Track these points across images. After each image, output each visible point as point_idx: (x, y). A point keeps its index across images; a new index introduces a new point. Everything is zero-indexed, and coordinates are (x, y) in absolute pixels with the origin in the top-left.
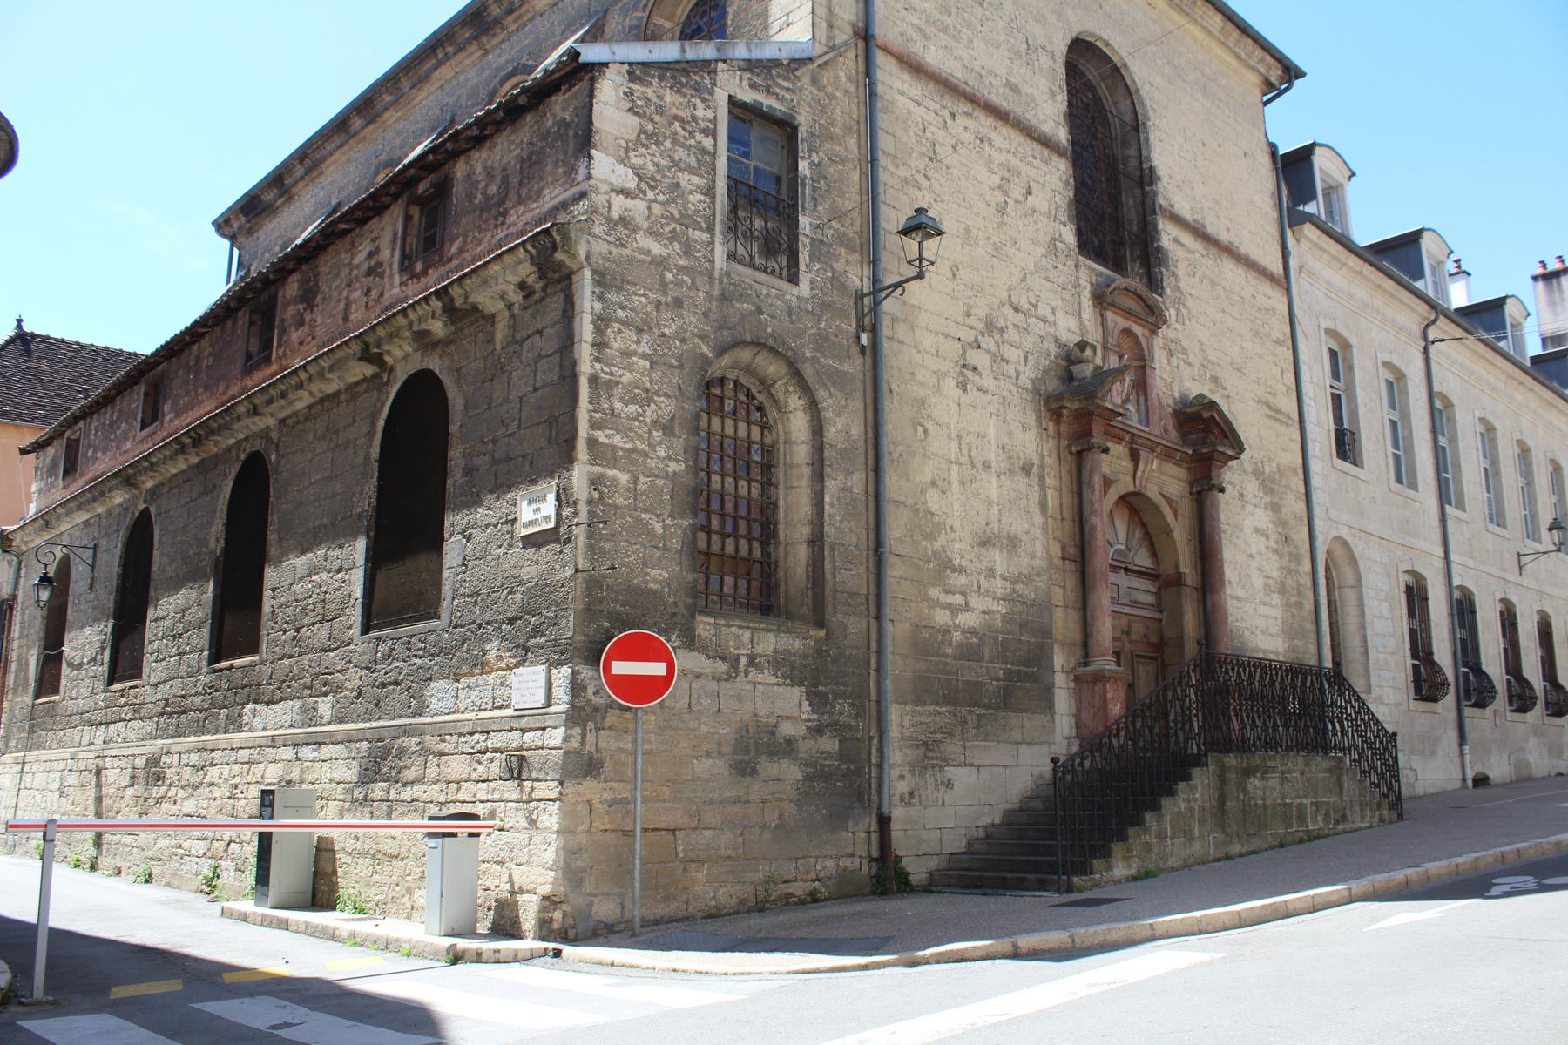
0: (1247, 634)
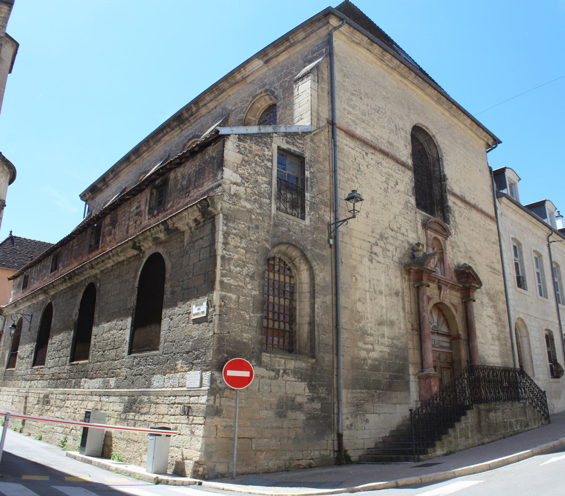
0: (486, 357)
